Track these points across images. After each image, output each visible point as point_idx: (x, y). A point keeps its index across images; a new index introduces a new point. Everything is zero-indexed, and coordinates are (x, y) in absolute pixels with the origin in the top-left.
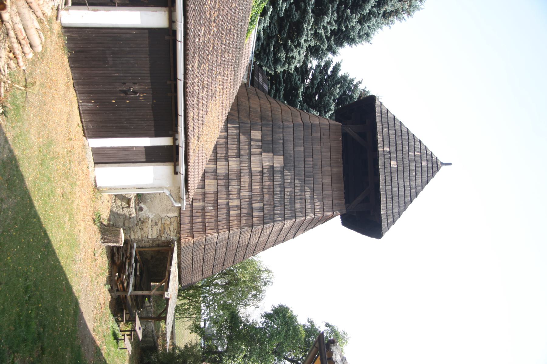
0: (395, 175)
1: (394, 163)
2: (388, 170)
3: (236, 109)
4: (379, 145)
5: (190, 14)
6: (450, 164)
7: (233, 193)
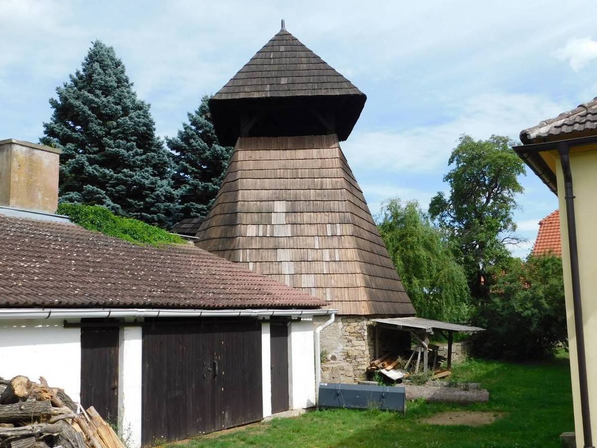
0: (297, 80)
1: (284, 81)
2: (291, 87)
3: (222, 252)
4: (264, 96)
5: (129, 300)
6: (283, 22)
7: (316, 256)
